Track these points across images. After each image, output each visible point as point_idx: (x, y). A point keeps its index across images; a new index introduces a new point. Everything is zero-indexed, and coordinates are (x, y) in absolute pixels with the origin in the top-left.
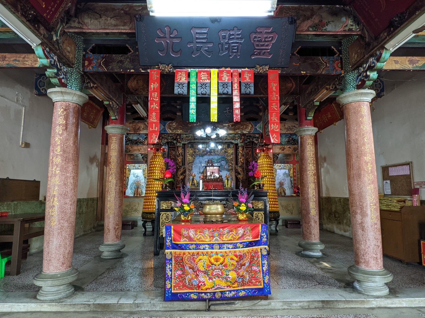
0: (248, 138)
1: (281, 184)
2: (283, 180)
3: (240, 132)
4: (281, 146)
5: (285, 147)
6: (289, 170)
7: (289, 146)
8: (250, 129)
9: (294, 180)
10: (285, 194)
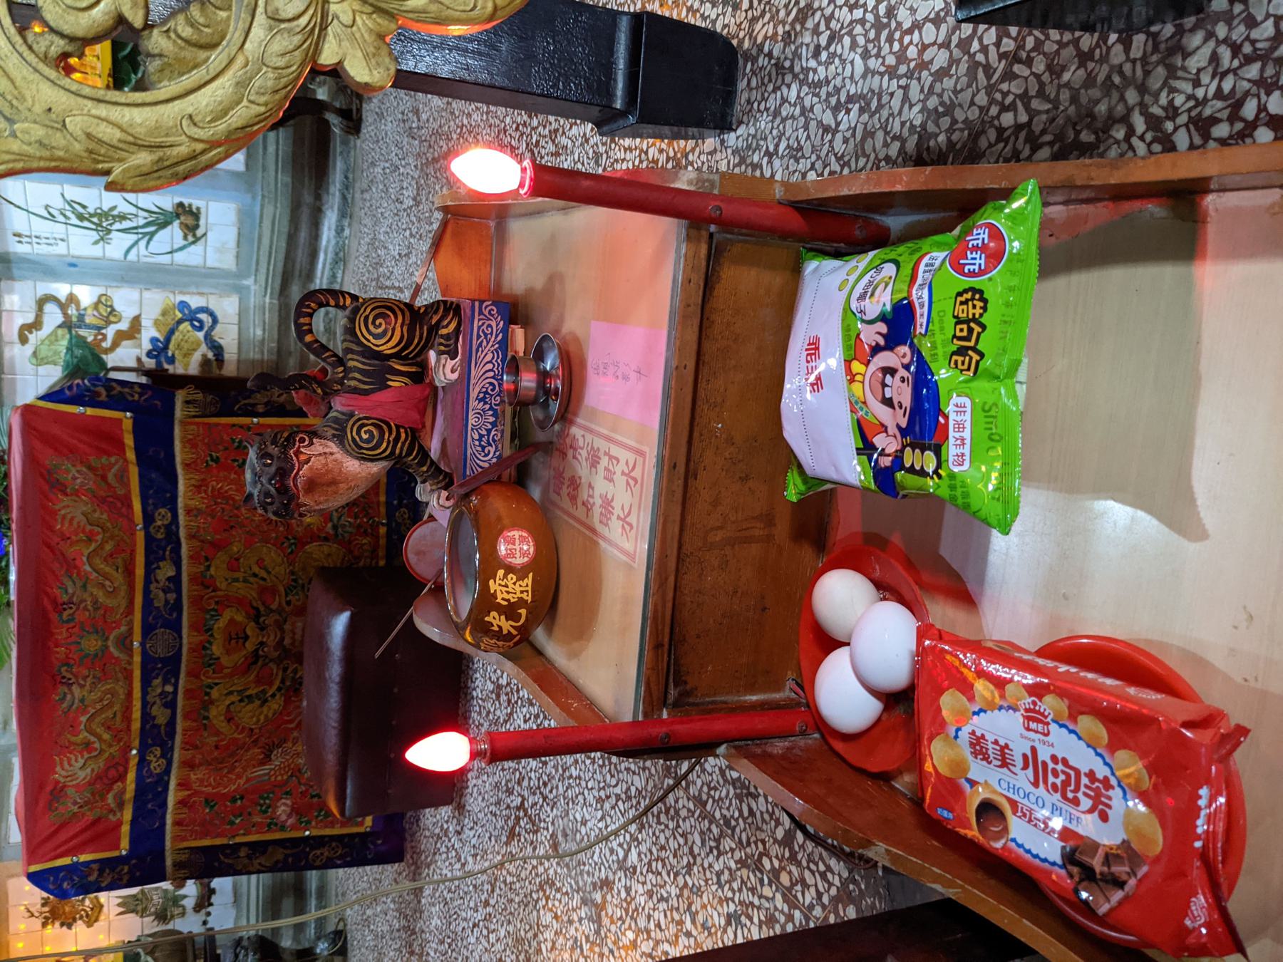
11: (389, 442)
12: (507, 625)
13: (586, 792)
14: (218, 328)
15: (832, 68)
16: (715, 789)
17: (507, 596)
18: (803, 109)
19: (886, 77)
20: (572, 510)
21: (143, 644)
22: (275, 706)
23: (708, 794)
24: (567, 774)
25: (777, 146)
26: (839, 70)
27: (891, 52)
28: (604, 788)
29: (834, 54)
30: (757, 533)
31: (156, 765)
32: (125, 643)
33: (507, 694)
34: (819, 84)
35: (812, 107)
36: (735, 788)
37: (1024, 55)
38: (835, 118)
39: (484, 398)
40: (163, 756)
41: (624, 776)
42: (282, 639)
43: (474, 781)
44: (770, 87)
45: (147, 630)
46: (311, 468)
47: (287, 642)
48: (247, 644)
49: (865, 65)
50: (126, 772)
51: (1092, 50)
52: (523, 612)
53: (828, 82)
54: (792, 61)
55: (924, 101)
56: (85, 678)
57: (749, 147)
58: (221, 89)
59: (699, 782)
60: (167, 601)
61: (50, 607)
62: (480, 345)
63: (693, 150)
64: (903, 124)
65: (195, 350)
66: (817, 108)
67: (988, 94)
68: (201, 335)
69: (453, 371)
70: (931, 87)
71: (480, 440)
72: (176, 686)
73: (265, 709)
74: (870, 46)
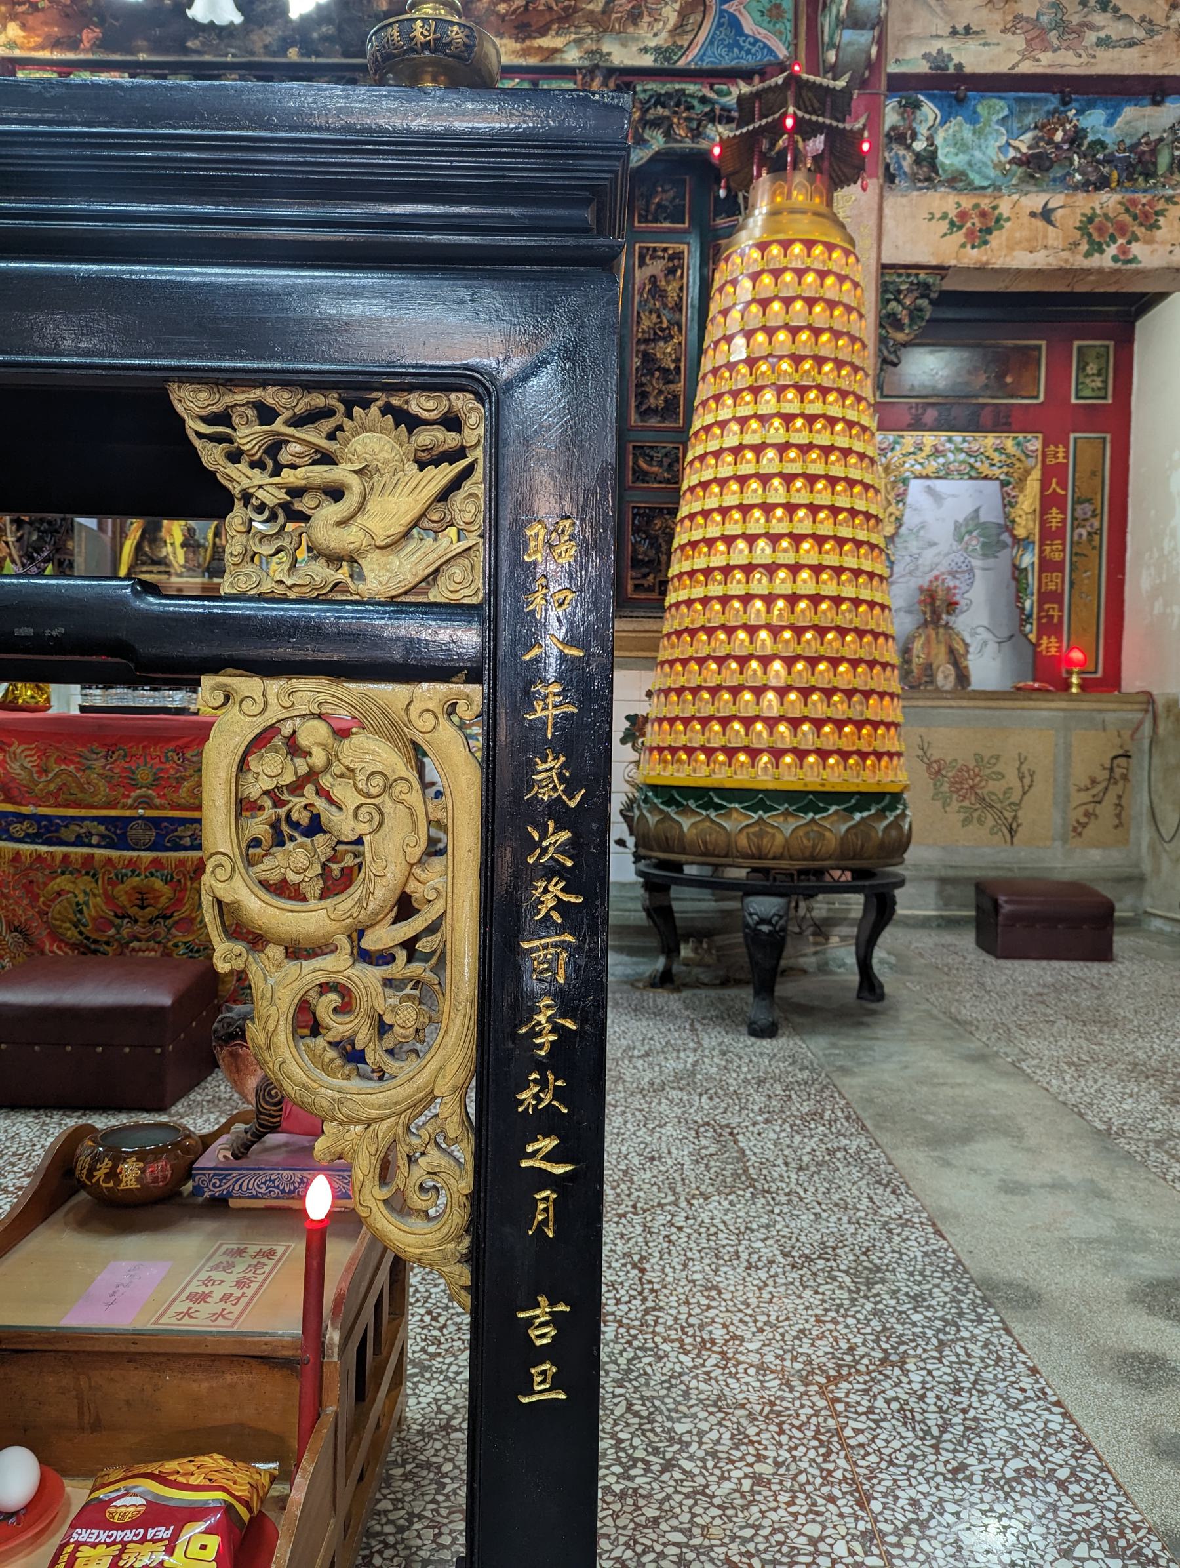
0: (656, 124)
1: (937, 607)
2: (953, 574)
3: (572, 57)
4: (967, 202)
5: (1005, 208)
6: (1009, 487)
7: (1036, 201)
8: (679, 29)
9: (1045, 565)
10: (963, 677)
12: (100, 1174)
21: (141, 818)
22: (69, 933)
30: (86, 1418)
31: (18, 829)
32: (148, 804)
40: (27, 835)
45: (155, 822)
47: (135, 944)
50: (15, 803)
52: (111, 1184)
56: (111, 770)
58: (301, 1076)
60: (181, 838)
61: (180, 743)
72: (98, 846)
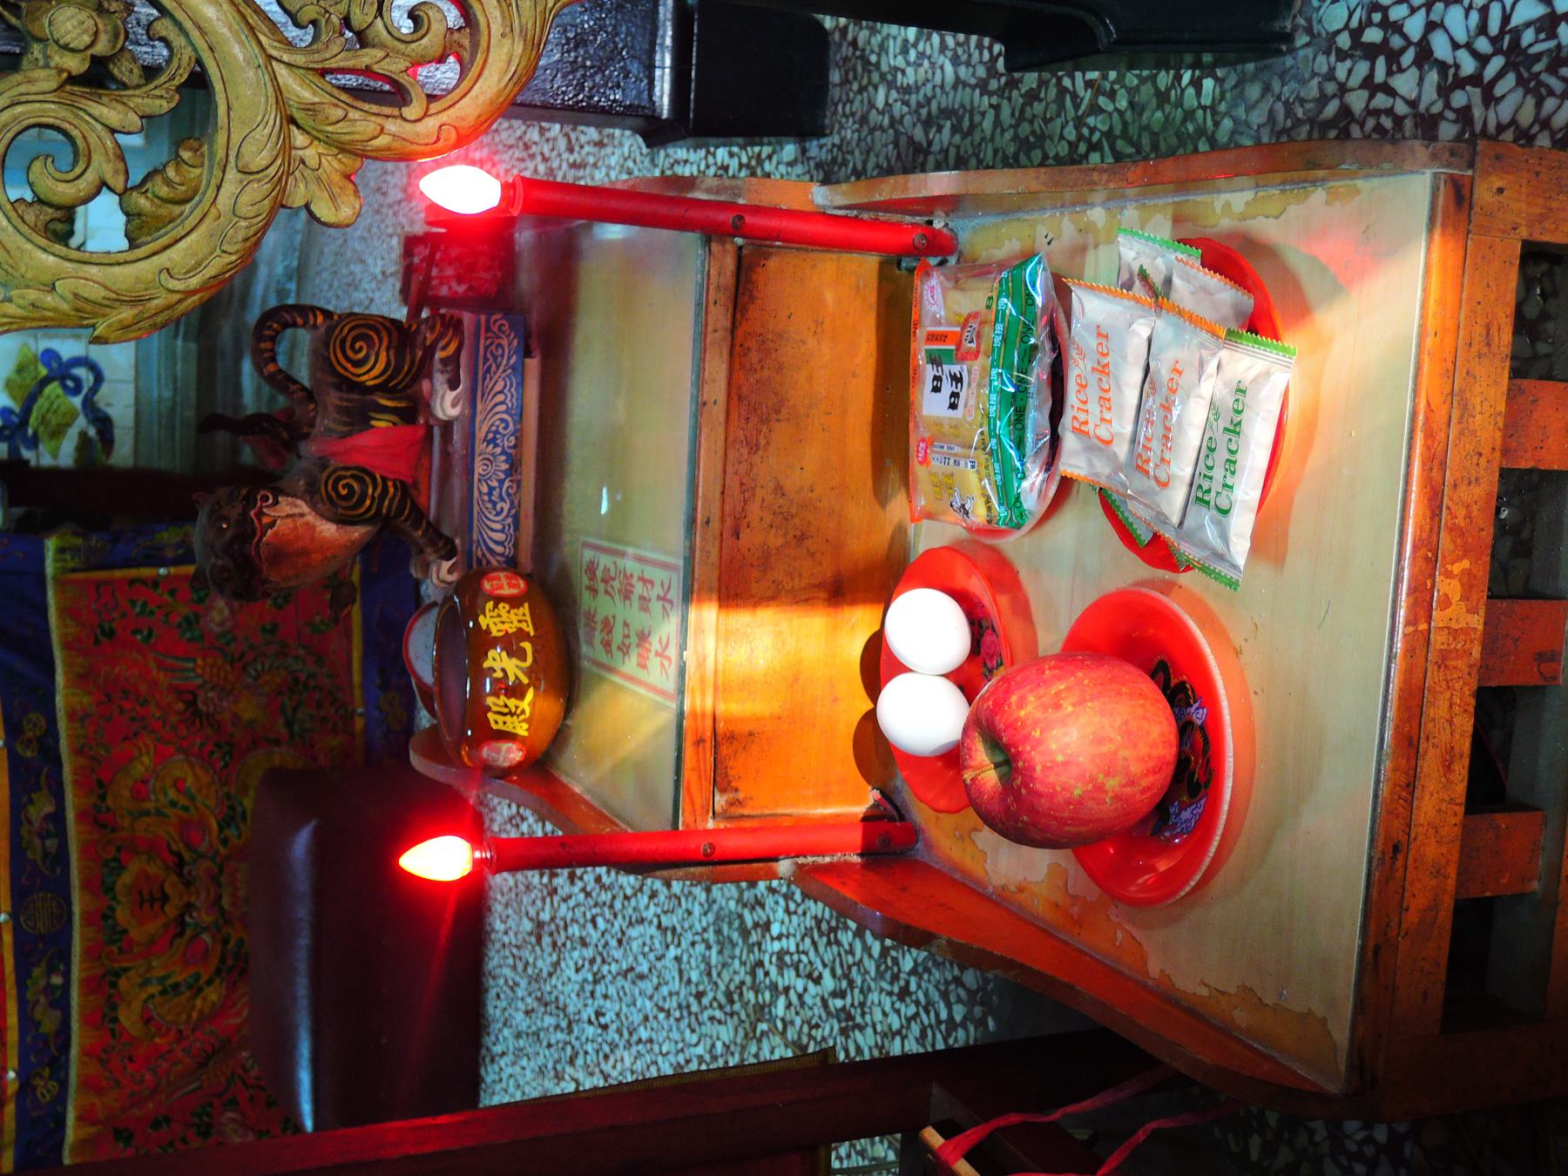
11: (373, 498)
13: (660, 1059)
14: (104, 389)
15: (921, 71)
16: (817, 1026)
17: (501, 626)
18: (892, 118)
19: (977, 91)
20: (641, 674)
22: (213, 997)
23: (810, 1036)
24: (635, 1038)
25: (865, 163)
26: (930, 75)
27: (981, 62)
28: (682, 1050)
29: (921, 55)
33: (551, 934)
34: (906, 90)
35: (902, 117)
36: (839, 1021)
37: (1108, 86)
38: (926, 133)
39: (494, 439)
41: (708, 1028)
42: (219, 898)
43: (509, 1070)
44: (855, 87)
46: (276, 534)
48: (167, 908)
49: (956, 73)
51: (1168, 90)
52: (527, 646)
53: (918, 89)
54: (879, 55)
55: (1016, 127)
57: (834, 160)
59: (798, 1021)
62: (488, 370)
63: (770, 157)
64: (996, 152)
65: (69, 425)
66: (907, 120)
67: (1077, 127)
68: (77, 401)
69: (454, 406)
70: (1022, 111)
71: (490, 494)
73: (198, 1002)
74: (960, 51)
